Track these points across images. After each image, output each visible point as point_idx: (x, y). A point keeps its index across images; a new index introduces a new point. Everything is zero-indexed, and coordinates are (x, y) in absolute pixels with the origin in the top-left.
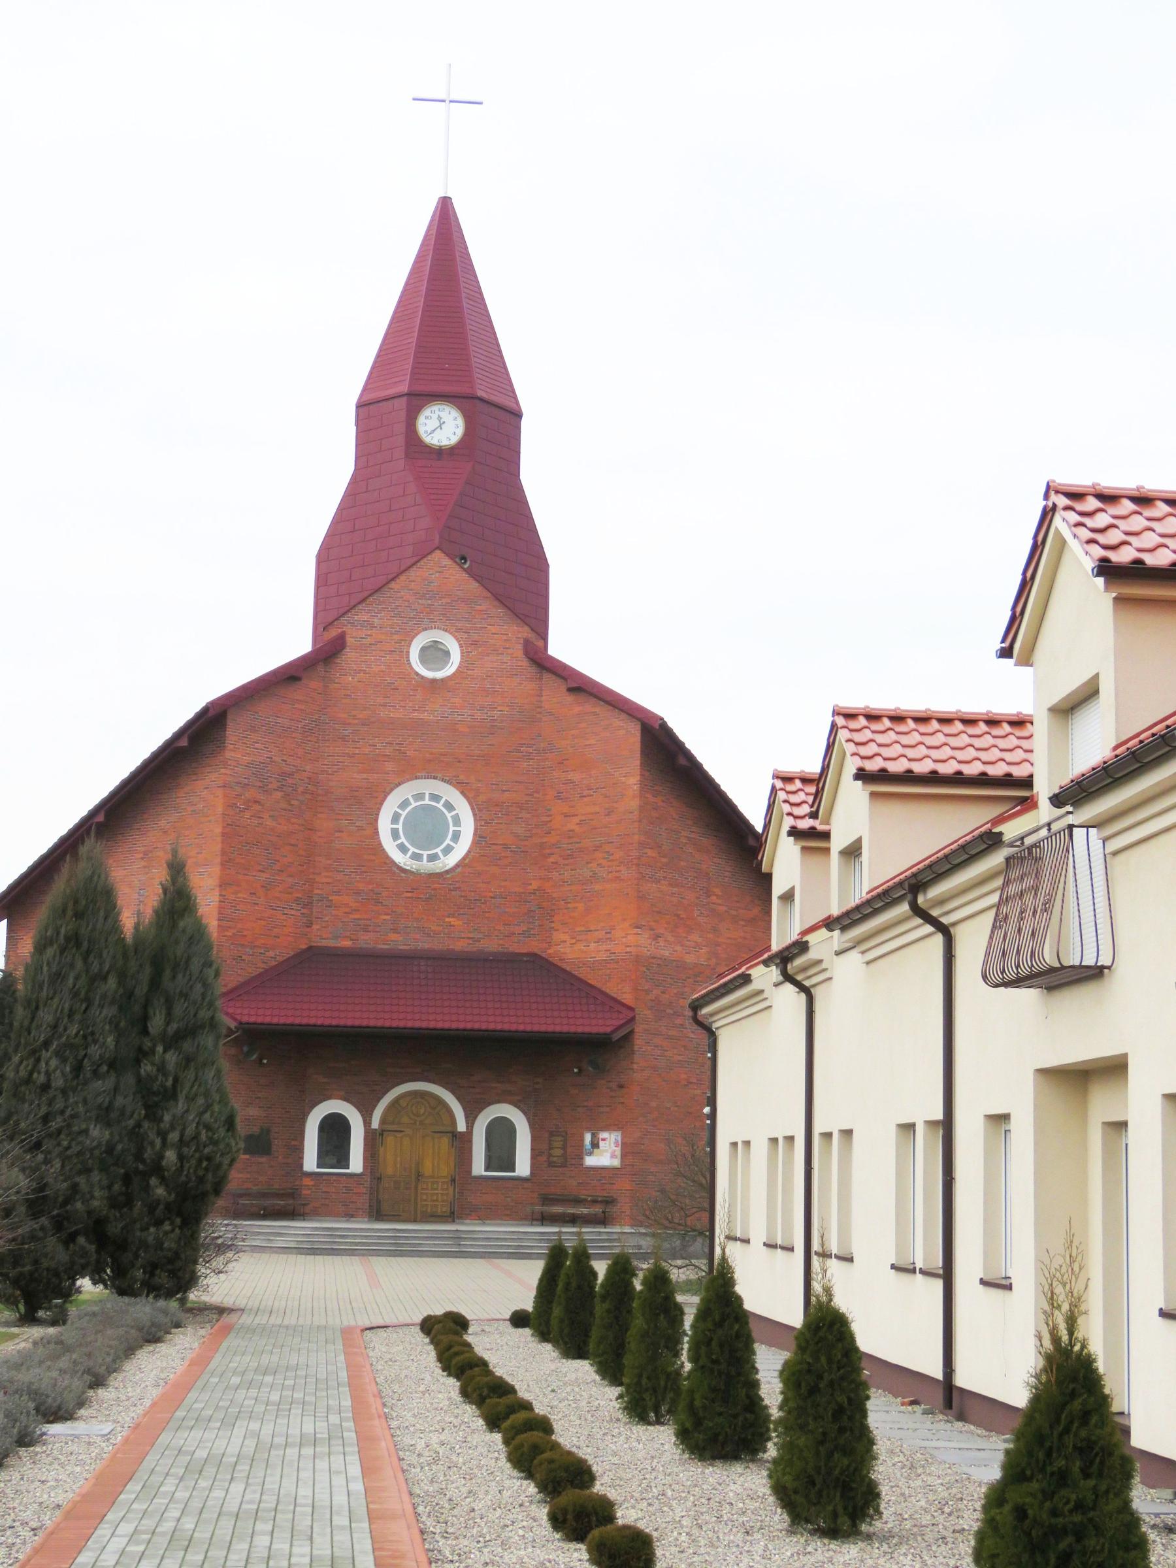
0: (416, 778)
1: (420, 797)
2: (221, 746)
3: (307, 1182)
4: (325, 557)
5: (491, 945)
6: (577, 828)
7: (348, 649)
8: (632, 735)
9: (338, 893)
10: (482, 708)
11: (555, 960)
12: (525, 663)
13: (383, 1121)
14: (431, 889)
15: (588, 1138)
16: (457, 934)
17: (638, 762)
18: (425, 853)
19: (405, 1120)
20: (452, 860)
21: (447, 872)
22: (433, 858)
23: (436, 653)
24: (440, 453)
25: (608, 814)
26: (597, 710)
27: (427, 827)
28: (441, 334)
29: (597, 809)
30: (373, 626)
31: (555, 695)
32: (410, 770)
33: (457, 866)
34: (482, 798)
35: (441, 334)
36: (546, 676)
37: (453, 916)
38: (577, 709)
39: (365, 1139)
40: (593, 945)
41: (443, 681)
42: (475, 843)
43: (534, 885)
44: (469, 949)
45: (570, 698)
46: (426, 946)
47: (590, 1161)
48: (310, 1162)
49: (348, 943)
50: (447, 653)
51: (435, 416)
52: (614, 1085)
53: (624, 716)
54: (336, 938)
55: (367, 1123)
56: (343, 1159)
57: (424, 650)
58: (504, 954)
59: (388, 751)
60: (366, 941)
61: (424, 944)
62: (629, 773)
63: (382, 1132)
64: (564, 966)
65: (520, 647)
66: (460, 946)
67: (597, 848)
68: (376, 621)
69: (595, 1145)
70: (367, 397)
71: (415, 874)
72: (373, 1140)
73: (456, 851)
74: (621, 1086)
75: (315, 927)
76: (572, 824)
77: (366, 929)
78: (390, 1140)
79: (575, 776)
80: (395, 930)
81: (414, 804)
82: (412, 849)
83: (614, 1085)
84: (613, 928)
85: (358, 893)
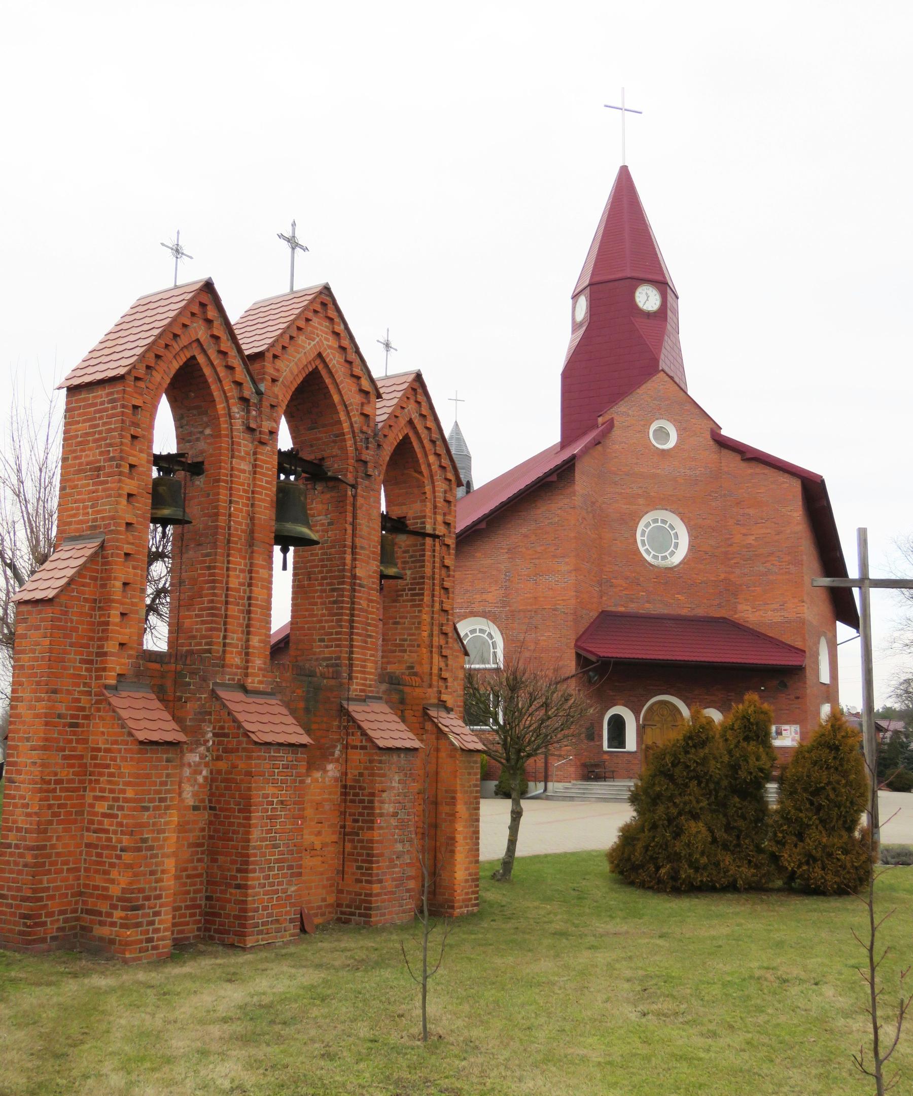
0: (656, 509)
1: (655, 521)
2: (572, 481)
3: (606, 757)
4: (567, 375)
5: (700, 612)
6: (753, 542)
7: (615, 429)
8: (796, 486)
9: (616, 578)
10: (690, 469)
11: (741, 622)
12: (712, 443)
13: (645, 719)
14: (667, 577)
15: (773, 728)
16: (682, 604)
17: (800, 503)
18: (660, 555)
19: (657, 718)
20: (649, 558)
21: (675, 567)
22: (664, 558)
23: (662, 434)
24: (648, 315)
25: (778, 534)
26: (766, 471)
27: (662, 540)
28: (625, 259)
29: (769, 531)
30: (628, 415)
31: (732, 462)
32: (655, 503)
33: (680, 563)
34: (692, 523)
35: (625, 259)
36: (725, 452)
37: (678, 594)
38: (750, 471)
39: (637, 730)
40: (770, 612)
41: (668, 450)
42: (690, 550)
43: (722, 576)
44: (689, 614)
45: (743, 465)
46: (666, 612)
47: (777, 743)
48: (605, 747)
49: (622, 609)
50: (668, 434)
51: (644, 293)
52: (792, 697)
53: (786, 475)
54: (615, 605)
55: (637, 720)
56: (622, 744)
57: (655, 431)
58: (705, 617)
59: (640, 491)
60: (633, 608)
61: (665, 611)
62: (795, 513)
63: (644, 726)
64: (748, 625)
65: (709, 433)
66: (685, 612)
67: (772, 554)
68: (630, 413)
69: (779, 733)
70: (597, 279)
71: (658, 567)
72: (641, 731)
73: (678, 551)
74: (798, 698)
75: (604, 598)
76: (751, 540)
77: (632, 601)
78: (648, 730)
79: (751, 512)
80: (648, 602)
81: (653, 525)
82: (653, 553)
83: (792, 697)
84: (785, 602)
85: (627, 578)
